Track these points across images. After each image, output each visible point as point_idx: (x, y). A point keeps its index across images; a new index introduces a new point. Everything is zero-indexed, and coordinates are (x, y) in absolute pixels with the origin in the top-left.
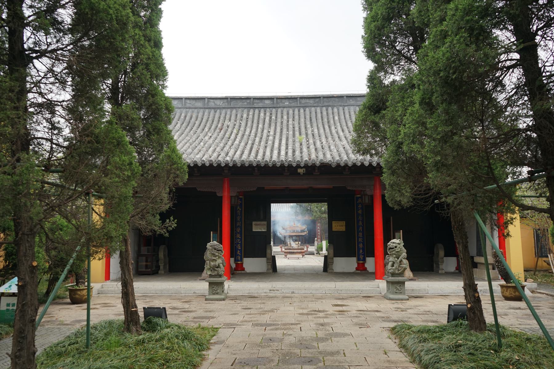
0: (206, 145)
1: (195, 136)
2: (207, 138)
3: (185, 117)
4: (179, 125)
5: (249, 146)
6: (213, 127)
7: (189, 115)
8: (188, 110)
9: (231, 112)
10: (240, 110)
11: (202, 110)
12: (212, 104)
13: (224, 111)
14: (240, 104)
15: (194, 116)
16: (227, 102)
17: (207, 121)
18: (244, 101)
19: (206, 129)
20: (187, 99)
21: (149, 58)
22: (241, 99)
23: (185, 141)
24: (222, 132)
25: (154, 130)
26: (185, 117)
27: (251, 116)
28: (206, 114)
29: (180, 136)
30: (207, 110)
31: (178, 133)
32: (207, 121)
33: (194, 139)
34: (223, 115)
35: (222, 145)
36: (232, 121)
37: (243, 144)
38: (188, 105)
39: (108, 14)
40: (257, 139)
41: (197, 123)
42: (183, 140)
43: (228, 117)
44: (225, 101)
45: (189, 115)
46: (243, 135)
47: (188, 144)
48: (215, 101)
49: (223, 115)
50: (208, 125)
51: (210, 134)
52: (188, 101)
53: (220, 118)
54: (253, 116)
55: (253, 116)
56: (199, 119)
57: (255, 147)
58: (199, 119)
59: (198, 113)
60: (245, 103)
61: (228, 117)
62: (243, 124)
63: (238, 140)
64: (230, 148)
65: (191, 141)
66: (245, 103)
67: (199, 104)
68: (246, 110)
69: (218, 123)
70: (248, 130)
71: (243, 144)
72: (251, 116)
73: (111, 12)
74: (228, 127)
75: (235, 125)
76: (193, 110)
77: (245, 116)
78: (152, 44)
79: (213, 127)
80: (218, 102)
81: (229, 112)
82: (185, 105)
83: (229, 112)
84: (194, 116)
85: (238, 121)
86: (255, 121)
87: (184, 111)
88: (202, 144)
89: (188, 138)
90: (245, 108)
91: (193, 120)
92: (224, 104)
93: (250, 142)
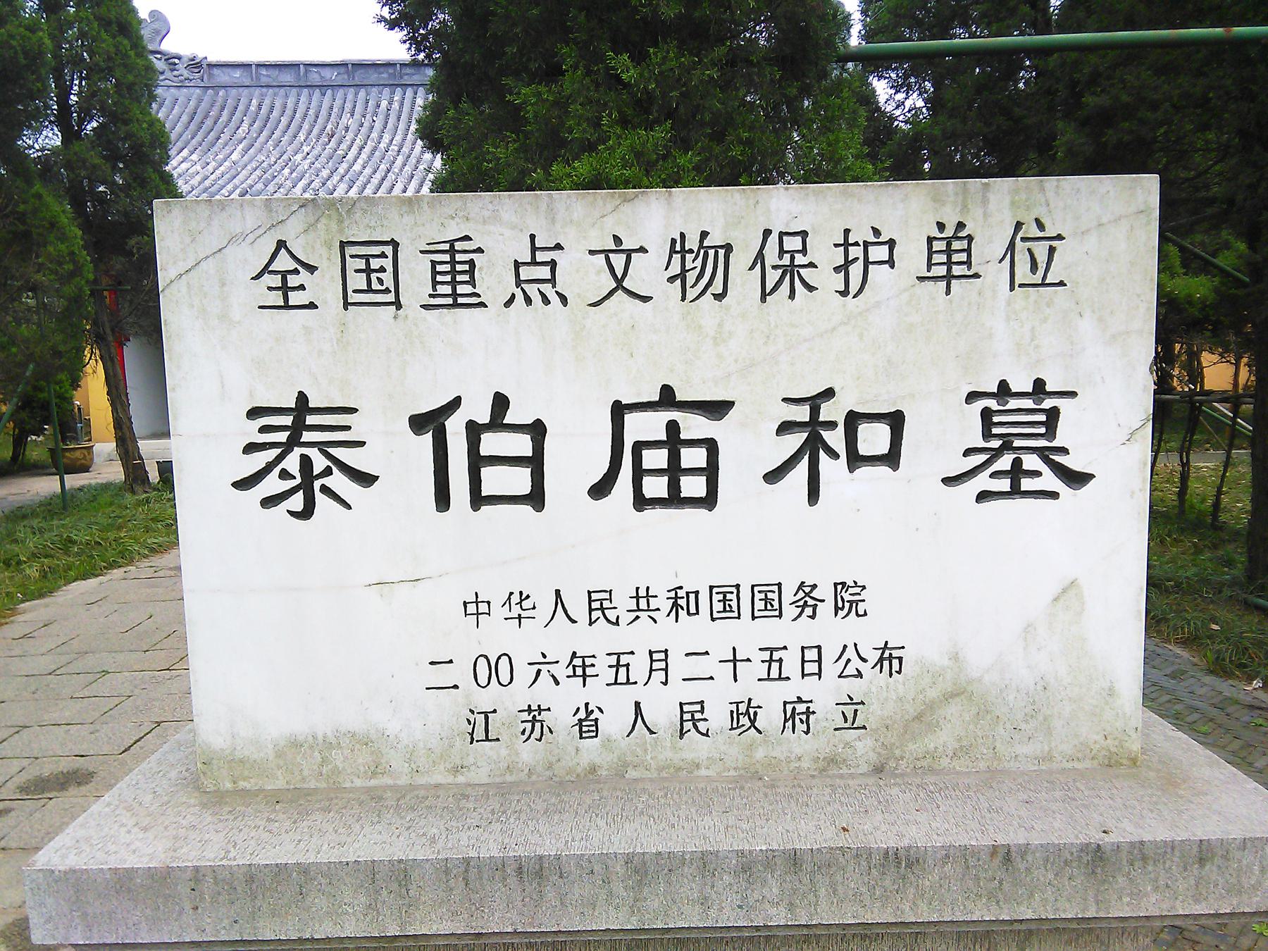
0: (294, 175)
1: (276, 153)
2: (299, 157)
3: (260, 106)
4: (245, 126)
5: (378, 176)
6: (315, 131)
7: (267, 102)
8: (264, 90)
9: (356, 94)
10: (375, 89)
11: (294, 91)
12: (314, 77)
13: (341, 92)
14: (373, 77)
15: (278, 104)
16: (347, 72)
17: (305, 115)
18: (382, 69)
19: (302, 136)
20: (259, 65)
21: (110, 59)
22: (374, 65)
23: (254, 164)
24: (333, 144)
25: (135, 179)
26: (260, 106)
27: (396, 106)
28: (303, 99)
29: (246, 151)
30: (306, 91)
31: (241, 146)
32: (305, 115)
33: (273, 159)
34: (338, 103)
35: (325, 173)
36: (357, 116)
37: (368, 171)
38: (264, 80)
39: (12, 47)
40: (400, 160)
41: (284, 120)
42: (250, 161)
43: (348, 106)
44: (342, 70)
45: (267, 102)
46: (375, 149)
47: (258, 172)
48: (319, 69)
49: (338, 103)
50: (306, 126)
51: (306, 149)
52: (264, 72)
53: (331, 108)
54: (402, 104)
55: (402, 104)
56: (289, 112)
57: (391, 176)
58: (289, 112)
59: (287, 96)
60: (385, 75)
61: (348, 106)
62: (378, 125)
63: (360, 161)
64: (341, 179)
65: (264, 165)
66: (385, 76)
67: (287, 77)
68: (387, 91)
69: (328, 120)
70: (398, 138)
71: (368, 171)
72: (396, 106)
73: (14, 43)
74: (347, 129)
75: (362, 126)
76: (276, 90)
77: (384, 104)
78: (115, 27)
79: (315, 131)
80: (327, 73)
81: (350, 97)
82: (258, 79)
83: (350, 97)
84: (278, 104)
85: (368, 116)
86: (404, 117)
87: (257, 91)
88: (286, 171)
89: (261, 157)
90: (386, 85)
91: (275, 113)
92: (340, 77)
93: (383, 167)
